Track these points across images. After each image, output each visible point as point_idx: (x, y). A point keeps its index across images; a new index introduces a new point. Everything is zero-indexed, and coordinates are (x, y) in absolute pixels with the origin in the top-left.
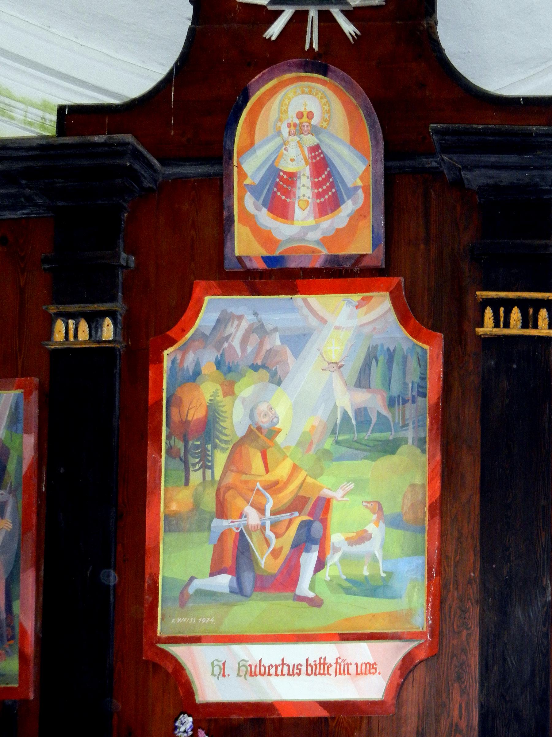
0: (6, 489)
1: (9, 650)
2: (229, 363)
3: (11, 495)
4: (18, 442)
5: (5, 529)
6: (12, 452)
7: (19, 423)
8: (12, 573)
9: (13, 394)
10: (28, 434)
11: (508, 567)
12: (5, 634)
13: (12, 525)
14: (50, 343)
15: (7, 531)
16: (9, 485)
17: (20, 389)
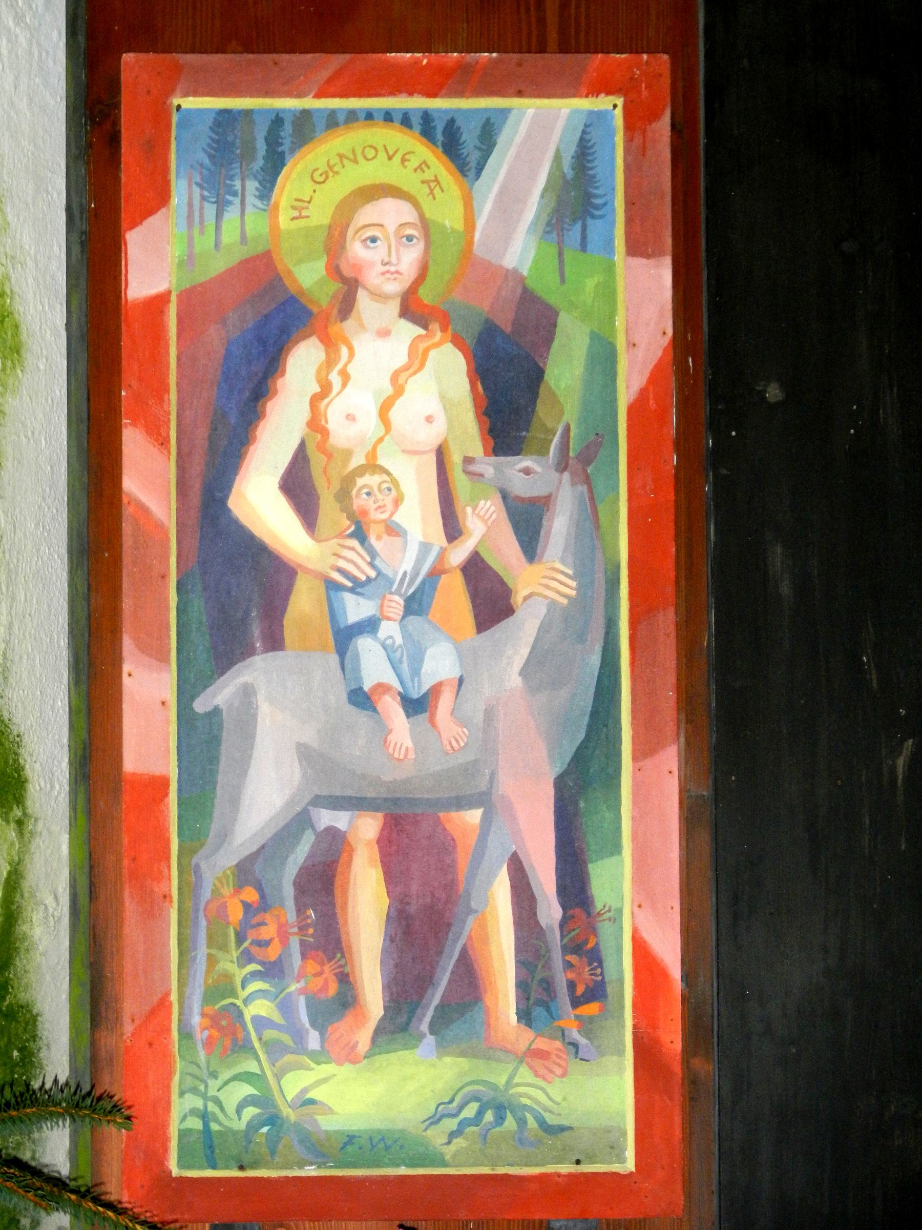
0: (543, 451)
1: (583, 1041)
2: (605, 195)
3: (566, 476)
4: (591, 284)
5: (546, 597)
6: (564, 320)
7: (593, 217)
8: (580, 759)
9: (565, 112)
10: (648, 256)
11: (81, 1091)
12: (561, 979)
13: (574, 584)
14: (80, 37)
15: (552, 605)
16: (556, 439)
17: (608, 93)
